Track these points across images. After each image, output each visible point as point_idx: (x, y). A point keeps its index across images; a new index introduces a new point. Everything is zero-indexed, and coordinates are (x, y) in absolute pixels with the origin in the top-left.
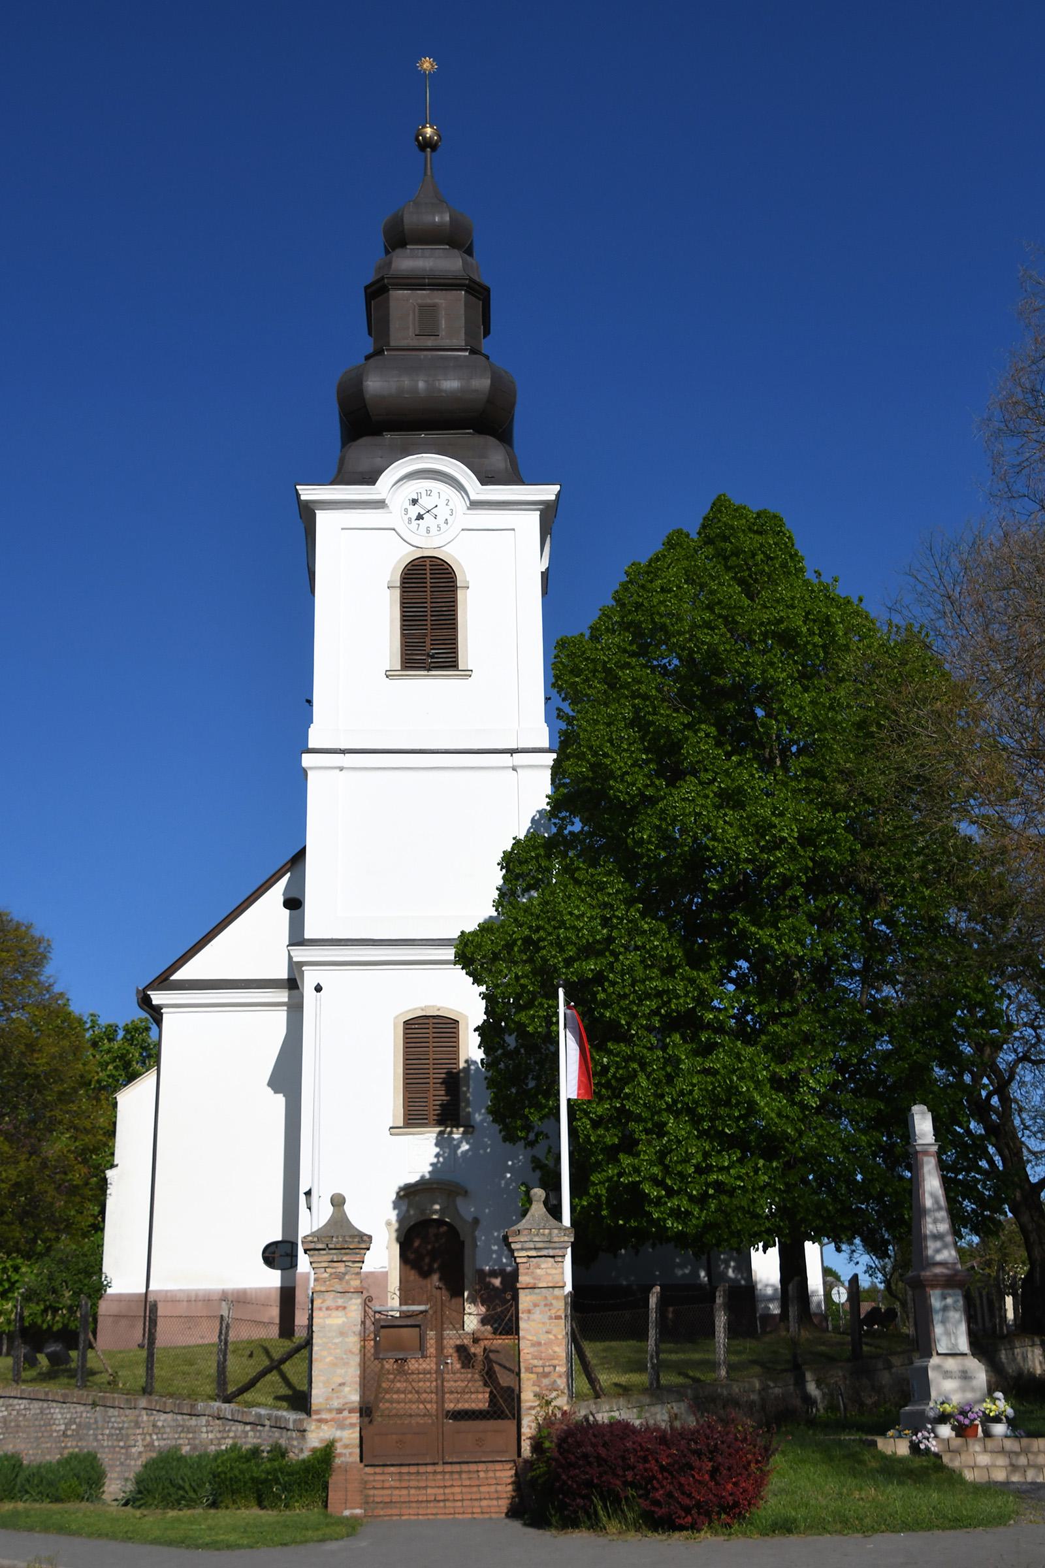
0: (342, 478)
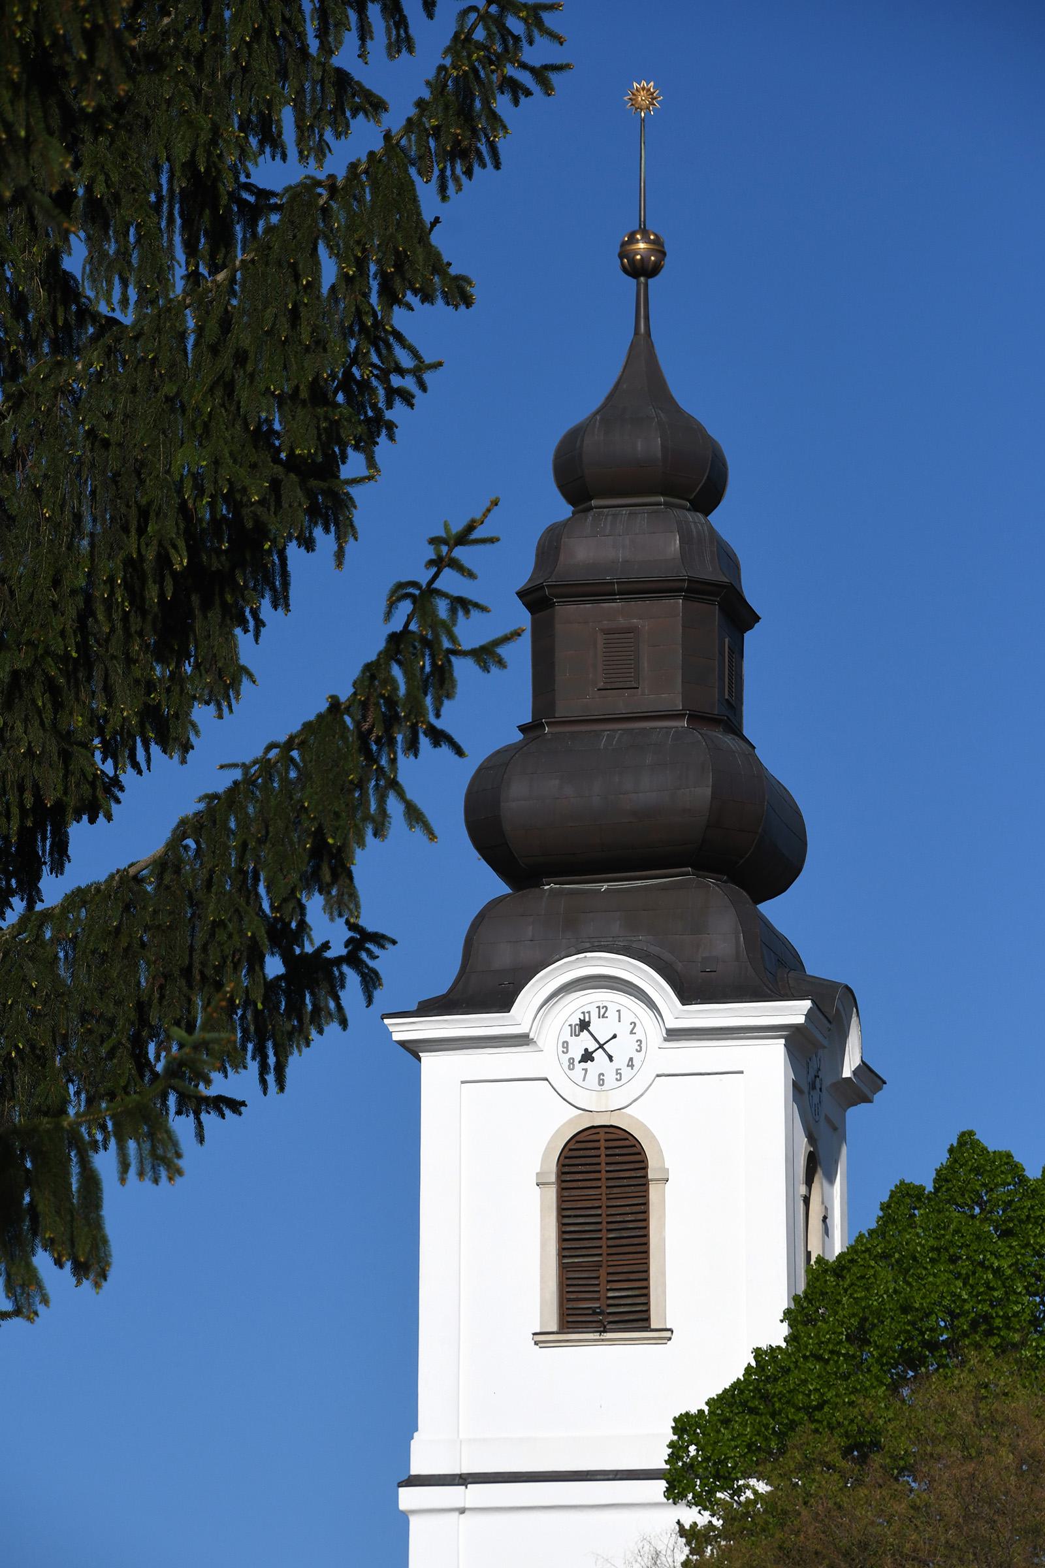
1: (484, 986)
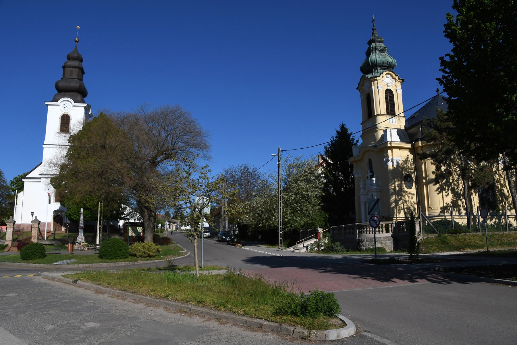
0: (52, 101)
1: (55, 100)
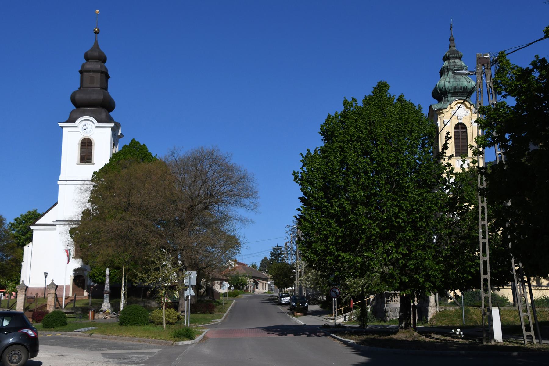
0: (68, 122)
1: (72, 120)
